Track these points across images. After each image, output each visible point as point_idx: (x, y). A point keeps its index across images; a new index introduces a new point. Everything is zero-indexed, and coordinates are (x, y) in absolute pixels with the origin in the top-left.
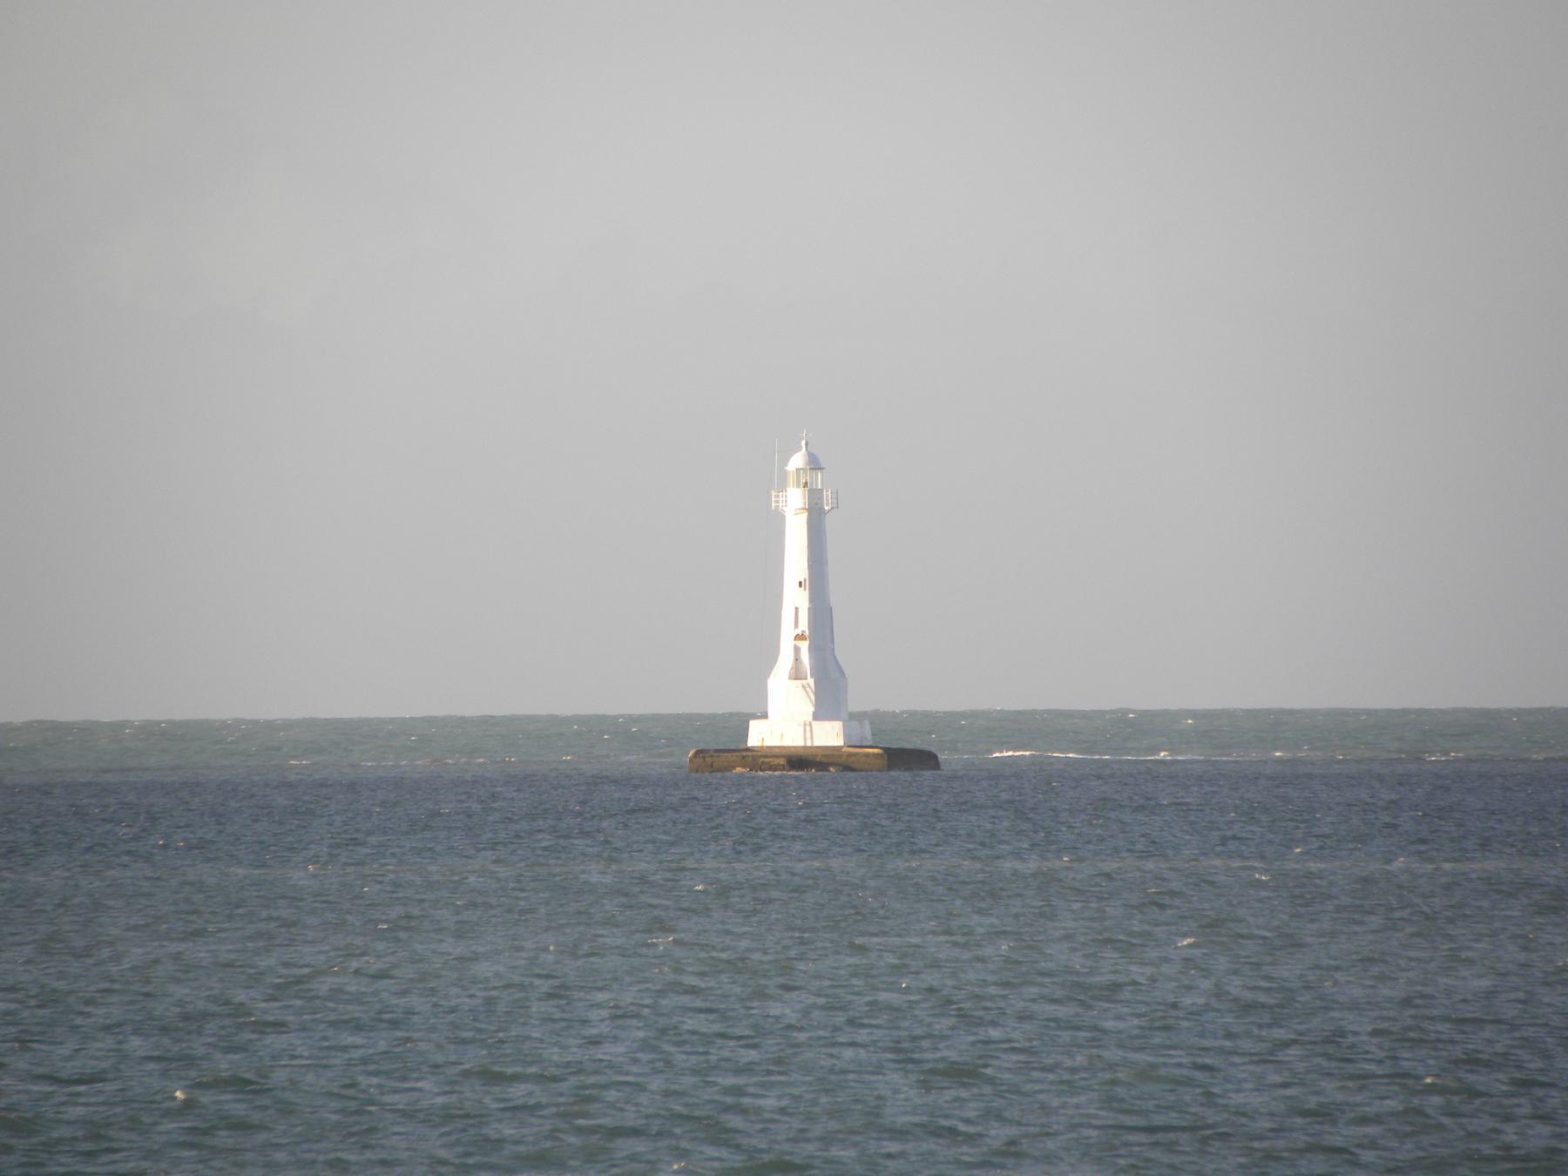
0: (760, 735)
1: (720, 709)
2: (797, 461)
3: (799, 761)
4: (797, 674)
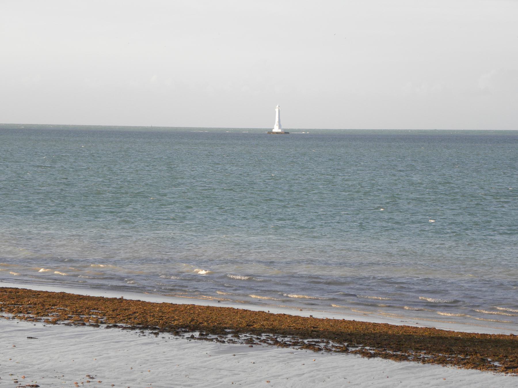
0: (274, 131)
1: (269, 128)
2: (277, 106)
3: (277, 133)
4: (277, 125)
